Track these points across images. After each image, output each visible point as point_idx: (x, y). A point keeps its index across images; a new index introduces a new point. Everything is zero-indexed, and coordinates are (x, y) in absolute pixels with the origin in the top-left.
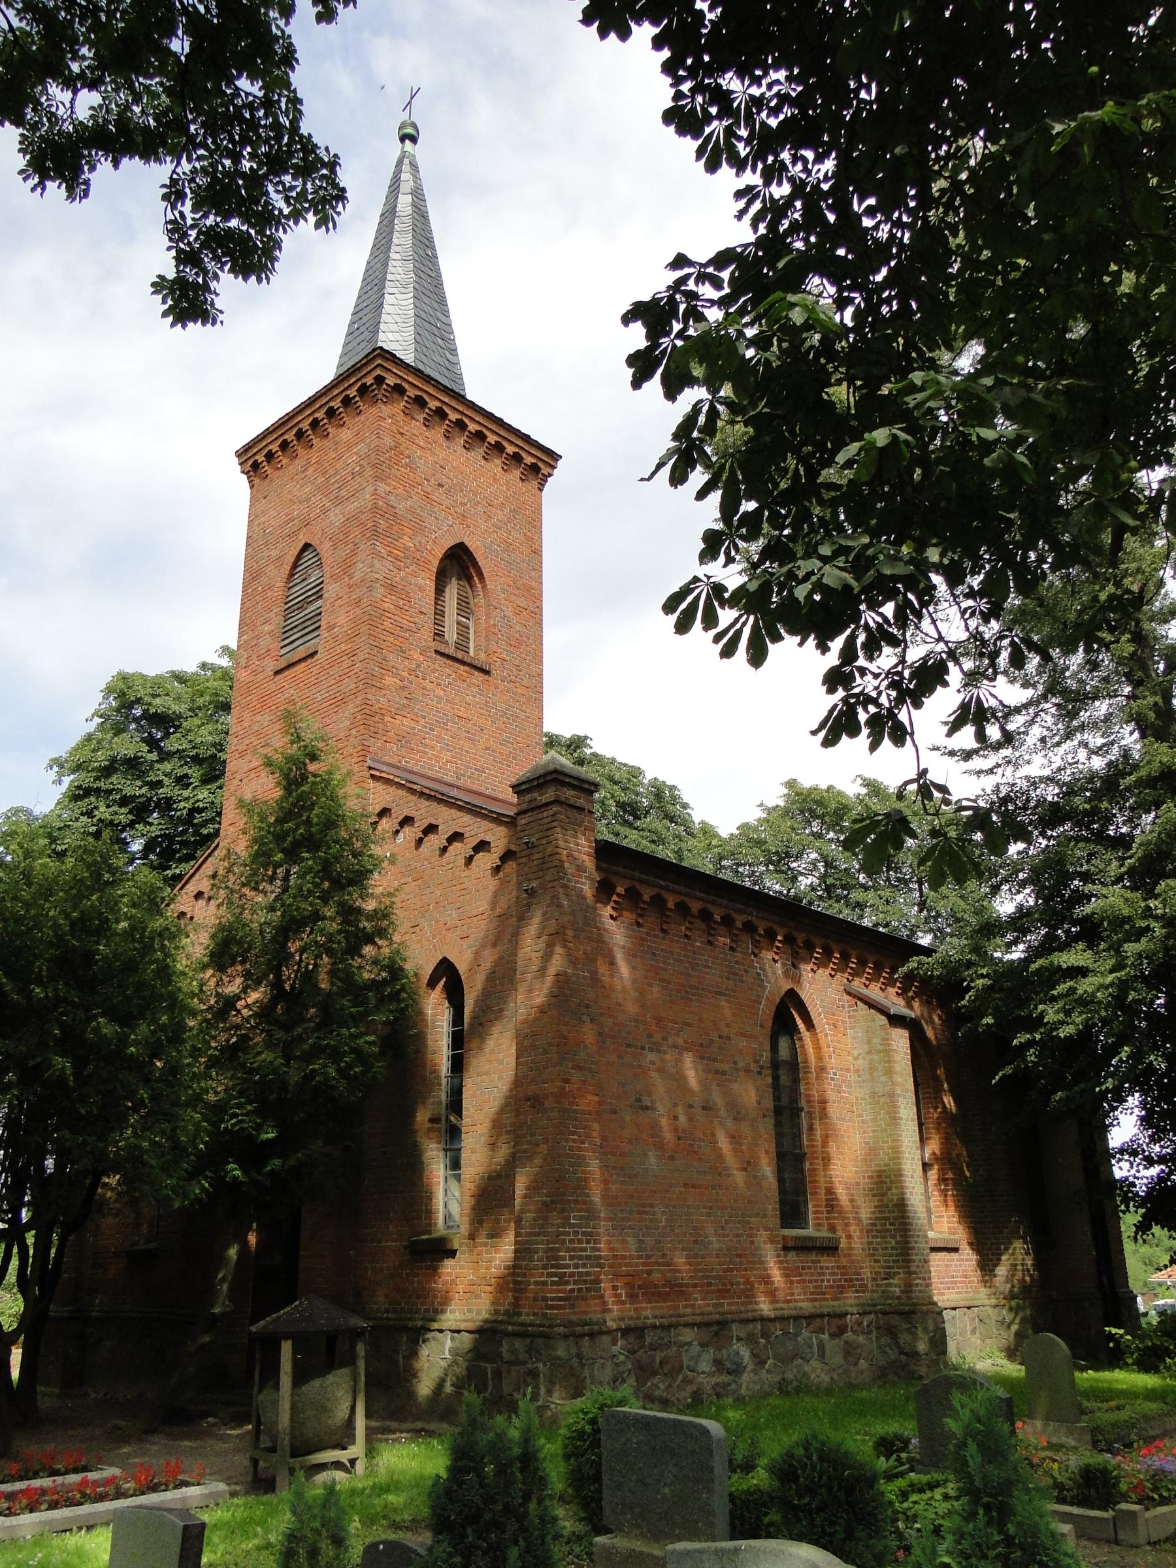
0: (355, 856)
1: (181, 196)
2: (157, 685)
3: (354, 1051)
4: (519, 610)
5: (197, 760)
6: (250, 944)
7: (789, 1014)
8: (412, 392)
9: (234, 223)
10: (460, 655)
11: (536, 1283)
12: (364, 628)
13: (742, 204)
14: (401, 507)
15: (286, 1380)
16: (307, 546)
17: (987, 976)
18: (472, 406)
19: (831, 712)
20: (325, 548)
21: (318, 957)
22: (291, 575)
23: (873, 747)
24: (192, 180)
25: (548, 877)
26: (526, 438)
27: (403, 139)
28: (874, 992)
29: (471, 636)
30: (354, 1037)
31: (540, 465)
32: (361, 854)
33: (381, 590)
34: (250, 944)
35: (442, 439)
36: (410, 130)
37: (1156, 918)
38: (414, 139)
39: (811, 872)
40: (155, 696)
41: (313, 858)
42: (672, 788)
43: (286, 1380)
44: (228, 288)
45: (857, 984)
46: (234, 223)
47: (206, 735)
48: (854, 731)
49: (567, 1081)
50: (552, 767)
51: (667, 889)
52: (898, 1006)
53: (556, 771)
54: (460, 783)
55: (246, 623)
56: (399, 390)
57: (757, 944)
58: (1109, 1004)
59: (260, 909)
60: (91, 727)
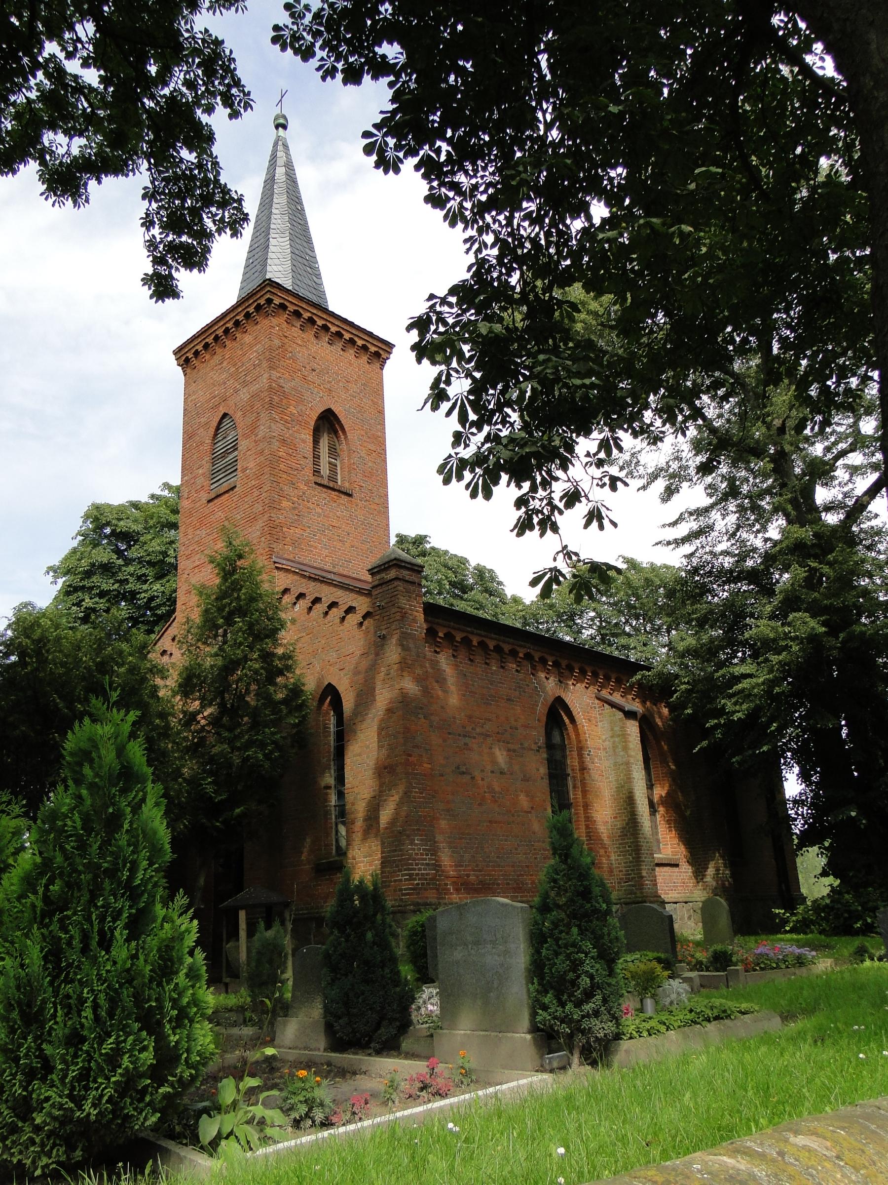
0: (269, 620)
1: (152, 223)
2: (120, 511)
3: (274, 742)
4: (370, 452)
5: (149, 563)
6: (206, 677)
7: (558, 715)
8: (291, 308)
9: (184, 238)
10: (331, 485)
11: (395, 881)
12: (267, 470)
13: (468, 245)
14: (287, 387)
15: (243, 934)
16: (225, 415)
17: (688, 683)
18: (333, 315)
19: (519, 520)
20: (238, 416)
21: (249, 684)
22: (216, 435)
23: (542, 535)
24: (158, 213)
25: (393, 627)
26: (370, 334)
27: (277, 127)
28: (617, 698)
29: (339, 471)
30: (273, 734)
31: (381, 352)
32: (273, 618)
33: (277, 444)
34: (206, 677)
35: (313, 339)
36: (282, 121)
37: (793, 639)
38: (285, 127)
39: (591, 626)
40: (120, 520)
41: (243, 621)
42: (491, 571)
43: (243, 934)
44: (184, 278)
45: (605, 693)
46: (184, 238)
47: (155, 546)
48: (532, 528)
49: (410, 755)
50: (393, 557)
51: (472, 633)
52: (636, 706)
53: (395, 559)
54: (335, 570)
55: (186, 469)
56: (283, 307)
57: (534, 668)
58: (762, 696)
59: (209, 657)
60: (75, 543)
